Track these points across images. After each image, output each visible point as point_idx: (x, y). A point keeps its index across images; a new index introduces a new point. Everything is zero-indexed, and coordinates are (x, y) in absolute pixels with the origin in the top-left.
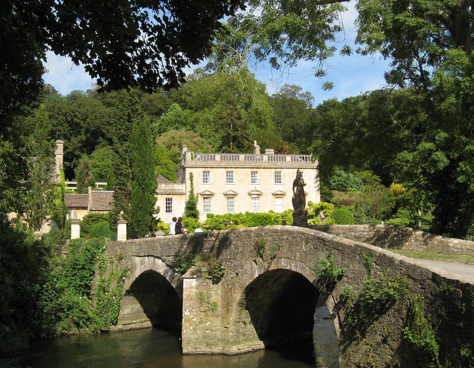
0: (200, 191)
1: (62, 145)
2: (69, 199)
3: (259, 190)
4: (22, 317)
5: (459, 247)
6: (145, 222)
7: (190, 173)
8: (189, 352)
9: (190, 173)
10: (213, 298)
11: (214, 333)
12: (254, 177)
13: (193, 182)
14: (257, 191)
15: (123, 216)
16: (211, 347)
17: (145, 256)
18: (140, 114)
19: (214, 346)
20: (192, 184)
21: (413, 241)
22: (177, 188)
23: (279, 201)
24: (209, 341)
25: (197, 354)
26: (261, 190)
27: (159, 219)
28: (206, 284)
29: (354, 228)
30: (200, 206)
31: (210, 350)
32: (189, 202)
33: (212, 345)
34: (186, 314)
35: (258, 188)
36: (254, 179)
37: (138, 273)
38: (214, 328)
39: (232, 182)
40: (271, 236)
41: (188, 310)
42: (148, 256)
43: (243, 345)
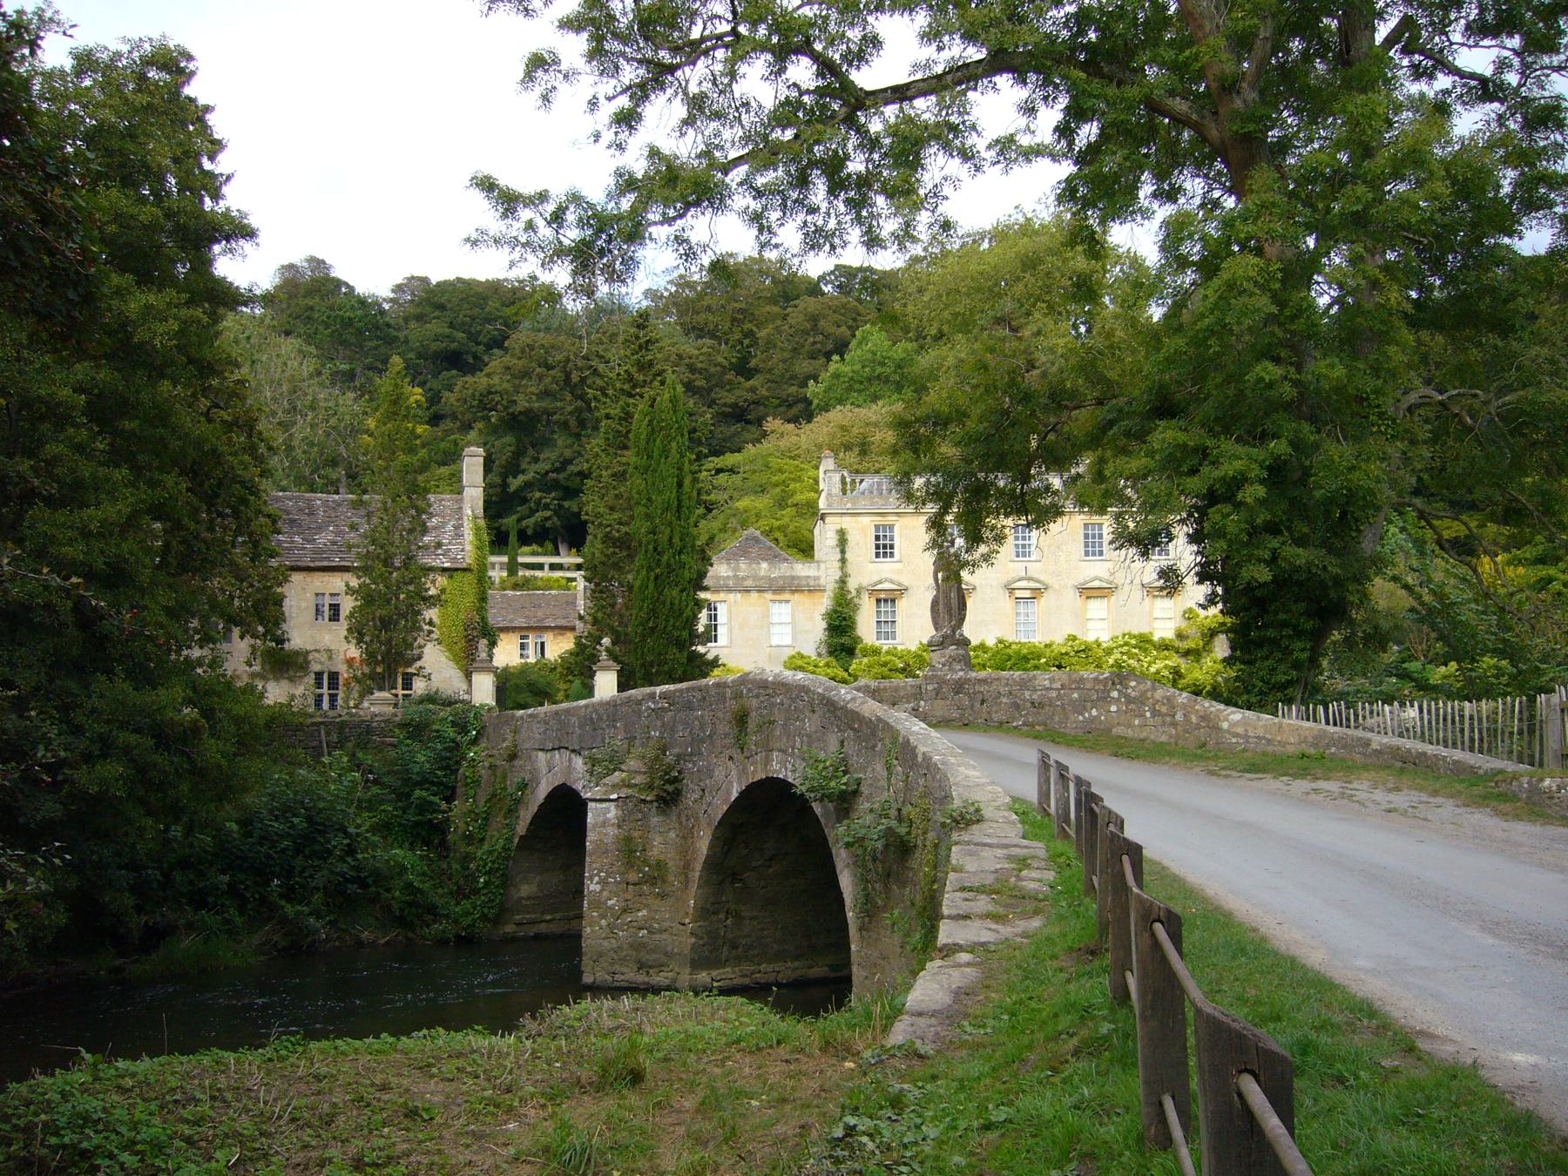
0: (866, 580)
1: (482, 459)
2: (540, 606)
3: (1036, 576)
4: (257, 896)
5: (1240, 730)
6: (666, 668)
7: (838, 531)
8: (598, 983)
9: (838, 531)
10: (655, 851)
11: (657, 937)
12: (1024, 538)
13: (848, 556)
14: (1030, 579)
15: (607, 650)
16: (648, 973)
17: (553, 749)
18: (659, 375)
19: (656, 970)
20: (843, 561)
21: (1148, 714)
22: (803, 574)
23: (1097, 607)
24: (648, 958)
25: (616, 989)
26: (1042, 578)
27: (716, 659)
28: (640, 816)
29: (1030, 680)
30: (866, 627)
31: (646, 979)
32: (835, 611)
33: (651, 967)
34: (592, 887)
35: (1035, 569)
36: (1024, 546)
37: (542, 791)
38: (656, 925)
39: (892, 555)
40: (757, 697)
41: (597, 879)
42: (559, 749)
43: (728, 969)
